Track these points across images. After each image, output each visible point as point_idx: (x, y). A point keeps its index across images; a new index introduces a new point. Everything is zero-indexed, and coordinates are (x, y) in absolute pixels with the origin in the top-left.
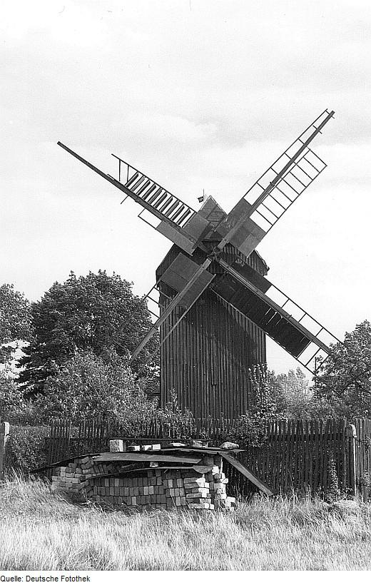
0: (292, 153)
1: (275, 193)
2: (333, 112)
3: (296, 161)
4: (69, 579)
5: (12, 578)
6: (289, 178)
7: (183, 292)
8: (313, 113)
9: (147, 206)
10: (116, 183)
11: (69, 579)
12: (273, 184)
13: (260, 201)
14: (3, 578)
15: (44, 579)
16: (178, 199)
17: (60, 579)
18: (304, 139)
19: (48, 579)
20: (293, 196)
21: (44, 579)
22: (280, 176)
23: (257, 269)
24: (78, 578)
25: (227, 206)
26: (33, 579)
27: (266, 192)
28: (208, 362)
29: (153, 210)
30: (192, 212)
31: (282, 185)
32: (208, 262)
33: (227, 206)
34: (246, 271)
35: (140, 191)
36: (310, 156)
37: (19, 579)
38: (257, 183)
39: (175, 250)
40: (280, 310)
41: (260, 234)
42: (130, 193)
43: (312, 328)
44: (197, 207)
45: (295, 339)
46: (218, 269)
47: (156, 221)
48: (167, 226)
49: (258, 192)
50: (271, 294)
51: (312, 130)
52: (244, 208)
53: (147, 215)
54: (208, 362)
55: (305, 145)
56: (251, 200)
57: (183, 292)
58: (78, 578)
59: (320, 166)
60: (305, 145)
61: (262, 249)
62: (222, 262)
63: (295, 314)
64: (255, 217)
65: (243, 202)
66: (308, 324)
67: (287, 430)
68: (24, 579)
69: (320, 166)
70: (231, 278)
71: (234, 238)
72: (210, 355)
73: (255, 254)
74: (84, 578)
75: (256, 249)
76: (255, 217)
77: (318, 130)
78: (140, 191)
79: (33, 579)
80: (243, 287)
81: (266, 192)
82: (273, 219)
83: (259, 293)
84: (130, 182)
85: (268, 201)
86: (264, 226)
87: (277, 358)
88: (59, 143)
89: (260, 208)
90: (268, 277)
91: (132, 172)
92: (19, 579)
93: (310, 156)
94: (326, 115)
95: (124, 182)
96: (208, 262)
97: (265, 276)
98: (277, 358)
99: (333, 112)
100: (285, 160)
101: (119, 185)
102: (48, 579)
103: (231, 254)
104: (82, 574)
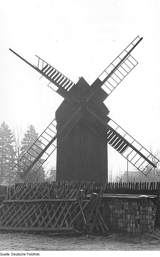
0: (122, 57)
1: (113, 76)
2: (142, 38)
3: (123, 61)
4: (31, 254)
5: (5, 254)
8: (131, 38)
9: (52, 80)
10: (37, 69)
12: (112, 72)
14: (1, 254)
15: (19, 255)
17: (26, 254)
18: (135, 43)
19: (21, 255)
20: (125, 74)
21: (19, 255)
22: (116, 68)
24: (34, 254)
26: (14, 254)
27: (109, 76)
29: (55, 83)
30: (73, 84)
31: (116, 72)
35: (48, 73)
37: (8, 254)
38: (115, 88)
41: (105, 95)
42: (44, 74)
43: (130, 140)
44: (76, 81)
45: (122, 145)
46: (84, 113)
47: (57, 88)
48: (61, 91)
50: (110, 124)
51: (132, 46)
52: (98, 83)
56: (102, 79)
58: (34, 254)
60: (129, 53)
61: (106, 102)
63: (122, 134)
64: (103, 87)
65: (98, 80)
66: (127, 138)
68: (11, 254)
69: (135, 63)
74: (37, 254)
76: (103, 87)
77: (135, 46)
78: (48, 73)
79: (14, 254)
81: (109, 76)
82: (112, 88)
84: (43, 69)
85: (110, 79)
86: (108, 91)
88: (10, 49)
89: (106, 83)
90: (109, 116)
91: (45, 65)
92: (8, 254)
96: (80, 108)
97: (107, 115)
98: (113, 156)
99: (142, 38)
102: (21, 255)
104: (36, 252)
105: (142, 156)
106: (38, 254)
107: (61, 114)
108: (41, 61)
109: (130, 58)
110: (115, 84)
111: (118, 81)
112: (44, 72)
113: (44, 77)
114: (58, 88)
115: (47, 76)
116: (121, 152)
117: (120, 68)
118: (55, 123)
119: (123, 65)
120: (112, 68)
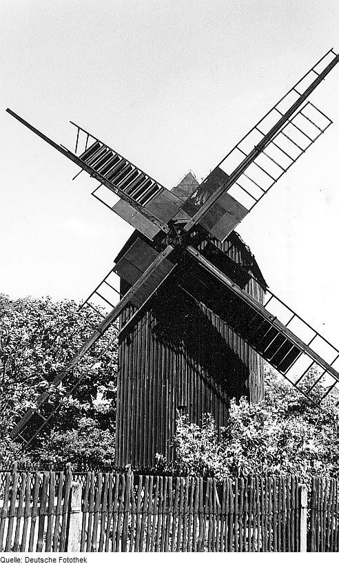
3: (290, 119)
5: (12, 559)
10: (68, 154)
12: (259, 149)
14: (3, 560)
15: (42, 561)
17: (58, 560)
18: (320, 69)
19: (47, 561)
21: (42, 561)
22: (286, 118)
23: (245, 267)
26: (31, 560)
28: (174, 377)
34: (220, 260)
35: (103, 164)
37: (18, 560)
39: (136, 234)
41: (240, 212)
43: (304, 335)
47: (229, 169)
51: (312, 77)
54: (174, 377)
55: (303, 97)
56: (229, 169)
59: (323, 123)
61: (244, 230)
64: (234, 191)
65: (217, 173)
67: (252, 533)
68: (23, 560)
69: (323, 123)
72: (177, 368)
73: (235, 239)
74: (81, 559)
75: (235, 230)
76: (234, 191)
77: (321, 77)
78: (103, 164)
79: (31, 560)
83: (237, 289)
85: (251, 170)
86: (246, 202)
88: (8, 110)
89: (242, 180)
91: (92, 142)
92: (18, 560)
102: (47, 561)
105: (259, 149)
106: (83, 560)
107: (125, 262)
108: (83, 136)
109: (309, 111)
111: (276, 172)
113: (85, 174)
114: (170, 187)
116: (299, 551)
117: (279, 139)
118: (115, 280)
119: (288, 129)
120: (256, 138)
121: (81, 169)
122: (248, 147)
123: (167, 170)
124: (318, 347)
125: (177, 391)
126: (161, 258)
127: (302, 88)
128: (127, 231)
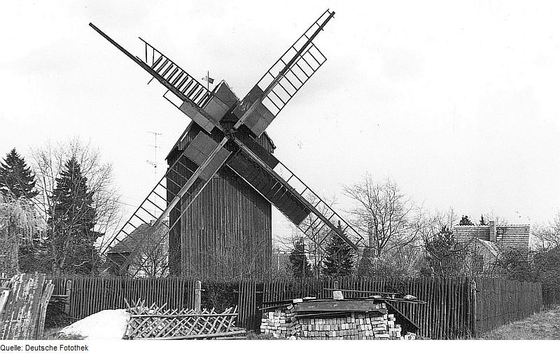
0: (287, 59)
2: (334, 13)
3: (302, 54)
4: (68, 348)
5: (12, 347)
6: (295, 69)
7: (204, 166)
9: (171, 87)
11: (68, 348)
12: (282, 73)
13: (268, 90)
14: (3, 348)
16: (193, 79)
18: (320, 22)
19: (47, 348)
22: (288, 67)
23: (265, 148)
24: (76, 348)
25: (241, 93)
27: (276, 81)
29: (176, 92)
31: (289, 75)
32: (225, 140)
33: (241, 93)
35: (163, 73)
36: (313, 50)
37: (18, 348)
38: (280, 110)
39: (194, 129)
40: (286, 185)
42: (155, 75)
45: (297, 208)
47: (179, 102)
48: (188, 105)
49: (268, 80)
50: (278, 170)
51: (316, 27)
52: (257, 94)
53: (171, 95)
55: (310, 41)
57: (204, 166)
58: (76, 348)
60: (310, 41)
61: (271, 131)
62: (237, 141)
64: (266, 102)
68: (24, 348)
69: (321, 60)
70: (245, 155)
71: (248, 119)
72: (224, 222)
73: (265, 134)
74: (83, 347)
76: (266, 102)
77: (321, 28)
78: (163, 73)
79: (32, 348)
80: (259, 166)
81: (276, 81)
83: (269, 169)
84: (155, 65)
85: (277, 88)
86: (274, 111)
87: (282, 229)
88: (91, 24)
89: (271, 95)
90: (276, 154)
91: (157, 56)
92: (18, 348)
93: (313, 50)
94: (327, 15)
95: (150, 64)
96: (225, 140)
98: (282, 229)
99: (334, 13)
100: (293, 53)
101: (147, 68)
102: (47, 348)
103: (245, 132)
108: (150, 50)
110: (147, 205)
112: (155, 69)
115: (161, 79)
118: (164, 182)
121: (152, 77)
122: (275, 72)
123: (202, 66)
124: (320, 208)
125: (224, 237)
126: (219, 147)
127: (309, 35)
128: (186, 121)
